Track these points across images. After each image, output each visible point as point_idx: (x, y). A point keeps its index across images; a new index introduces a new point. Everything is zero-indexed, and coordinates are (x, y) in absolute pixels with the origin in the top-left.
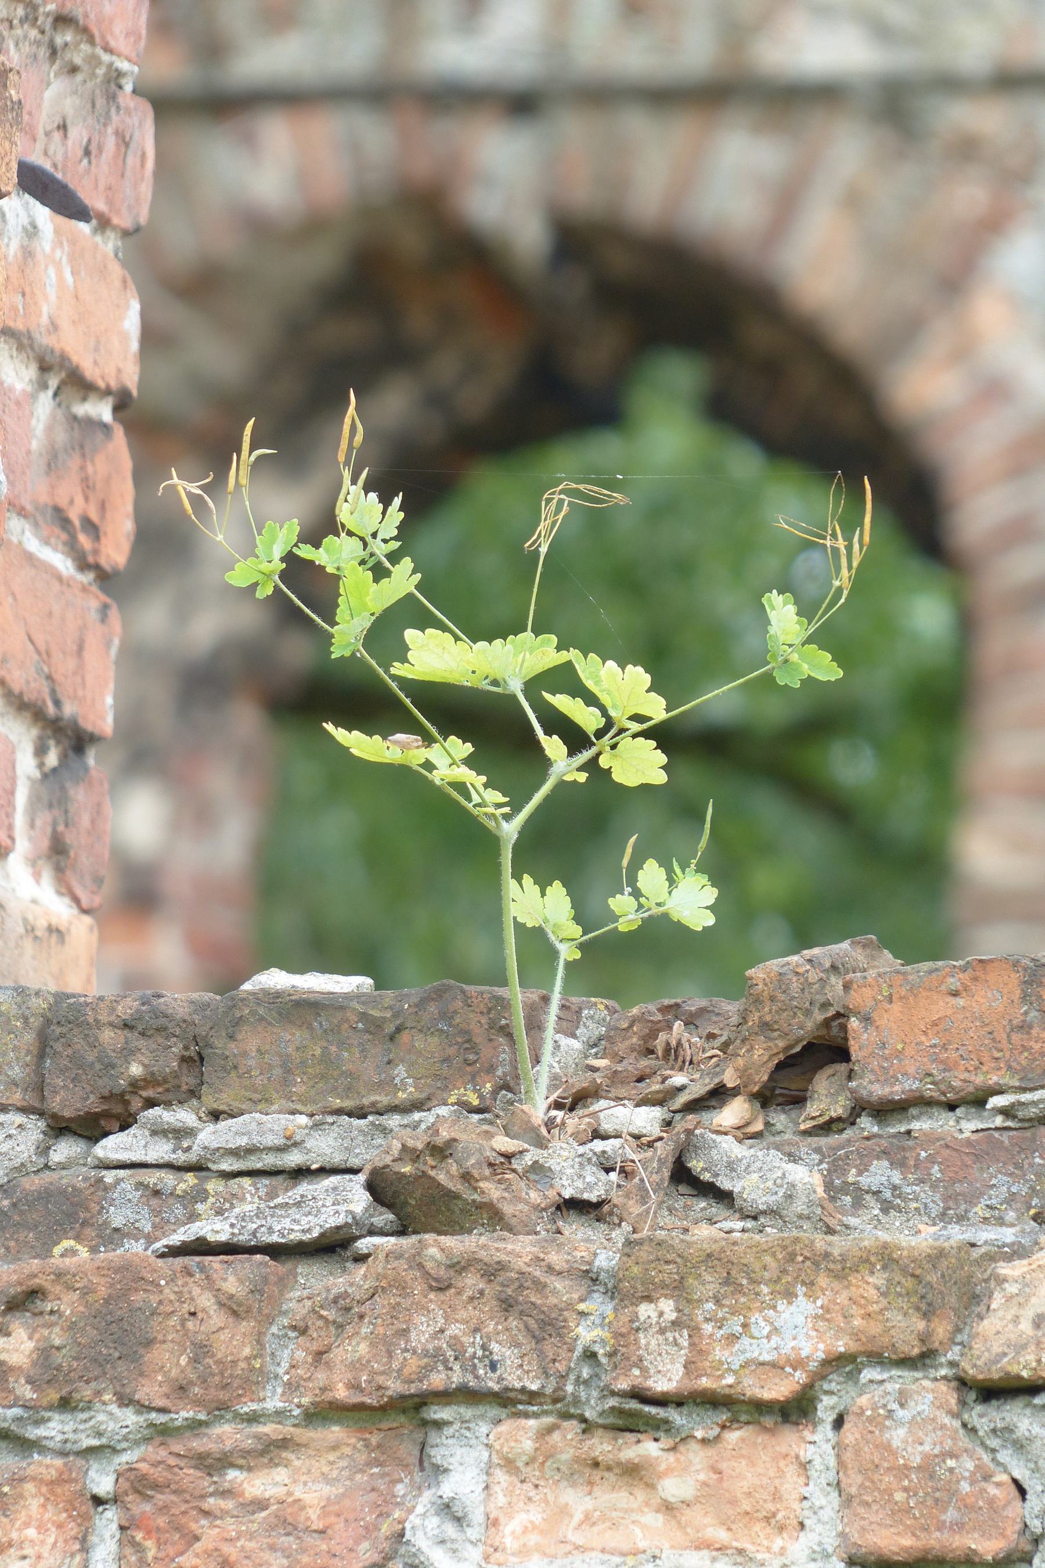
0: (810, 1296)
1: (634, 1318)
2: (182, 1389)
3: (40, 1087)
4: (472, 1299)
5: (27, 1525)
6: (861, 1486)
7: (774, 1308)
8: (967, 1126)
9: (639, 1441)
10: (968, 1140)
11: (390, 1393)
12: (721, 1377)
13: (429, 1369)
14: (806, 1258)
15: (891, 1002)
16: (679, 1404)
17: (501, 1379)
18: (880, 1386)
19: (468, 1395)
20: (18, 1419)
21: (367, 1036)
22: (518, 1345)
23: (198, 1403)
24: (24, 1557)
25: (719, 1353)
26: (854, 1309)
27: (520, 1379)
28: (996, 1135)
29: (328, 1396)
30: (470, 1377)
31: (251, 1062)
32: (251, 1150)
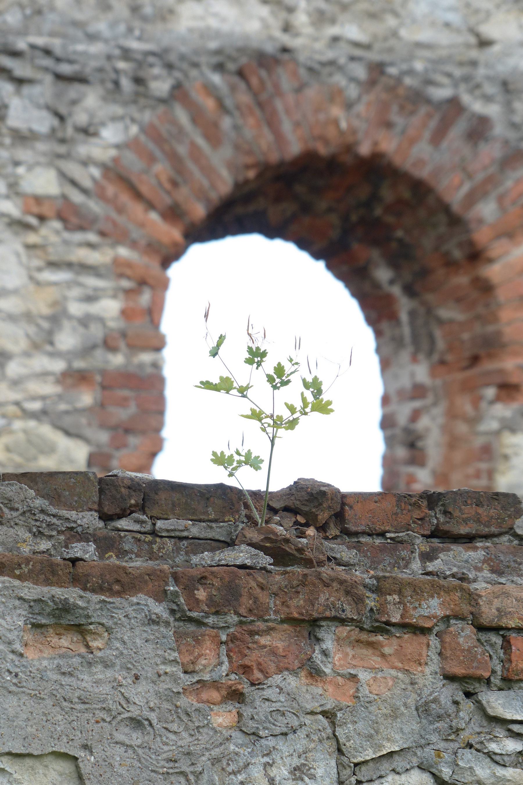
0: (439, 598)
1: (386, 600)
2: (250, 611)
3: (100, 504)
4: (336, 590)
5: (206, 649)
6: (451, 654)
7: (428, 600)
8: (378, 541)
9: (376, 636)
10: (378, 545)
11: (314, 617)
12: (413, 619)
13: (325, 610)
14: (437, 586)
15: (358, 502)
16: (394, 626)
17: (346, 615)
18: (456, 625)
19: (335, 619)
20: (203, 616)
21: (200, 498)
22: (351, 605)
23: (255, 615)
24: (206, 659)
25: (412, 612)
26: (451, 603)
27: (351, 615)
28: (386, 544)
29: (291, 616)
30: (337, 614)
31: (163, 502)
32: (175, 530)
